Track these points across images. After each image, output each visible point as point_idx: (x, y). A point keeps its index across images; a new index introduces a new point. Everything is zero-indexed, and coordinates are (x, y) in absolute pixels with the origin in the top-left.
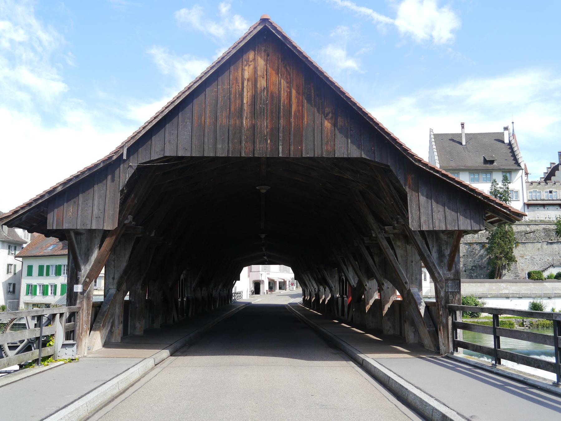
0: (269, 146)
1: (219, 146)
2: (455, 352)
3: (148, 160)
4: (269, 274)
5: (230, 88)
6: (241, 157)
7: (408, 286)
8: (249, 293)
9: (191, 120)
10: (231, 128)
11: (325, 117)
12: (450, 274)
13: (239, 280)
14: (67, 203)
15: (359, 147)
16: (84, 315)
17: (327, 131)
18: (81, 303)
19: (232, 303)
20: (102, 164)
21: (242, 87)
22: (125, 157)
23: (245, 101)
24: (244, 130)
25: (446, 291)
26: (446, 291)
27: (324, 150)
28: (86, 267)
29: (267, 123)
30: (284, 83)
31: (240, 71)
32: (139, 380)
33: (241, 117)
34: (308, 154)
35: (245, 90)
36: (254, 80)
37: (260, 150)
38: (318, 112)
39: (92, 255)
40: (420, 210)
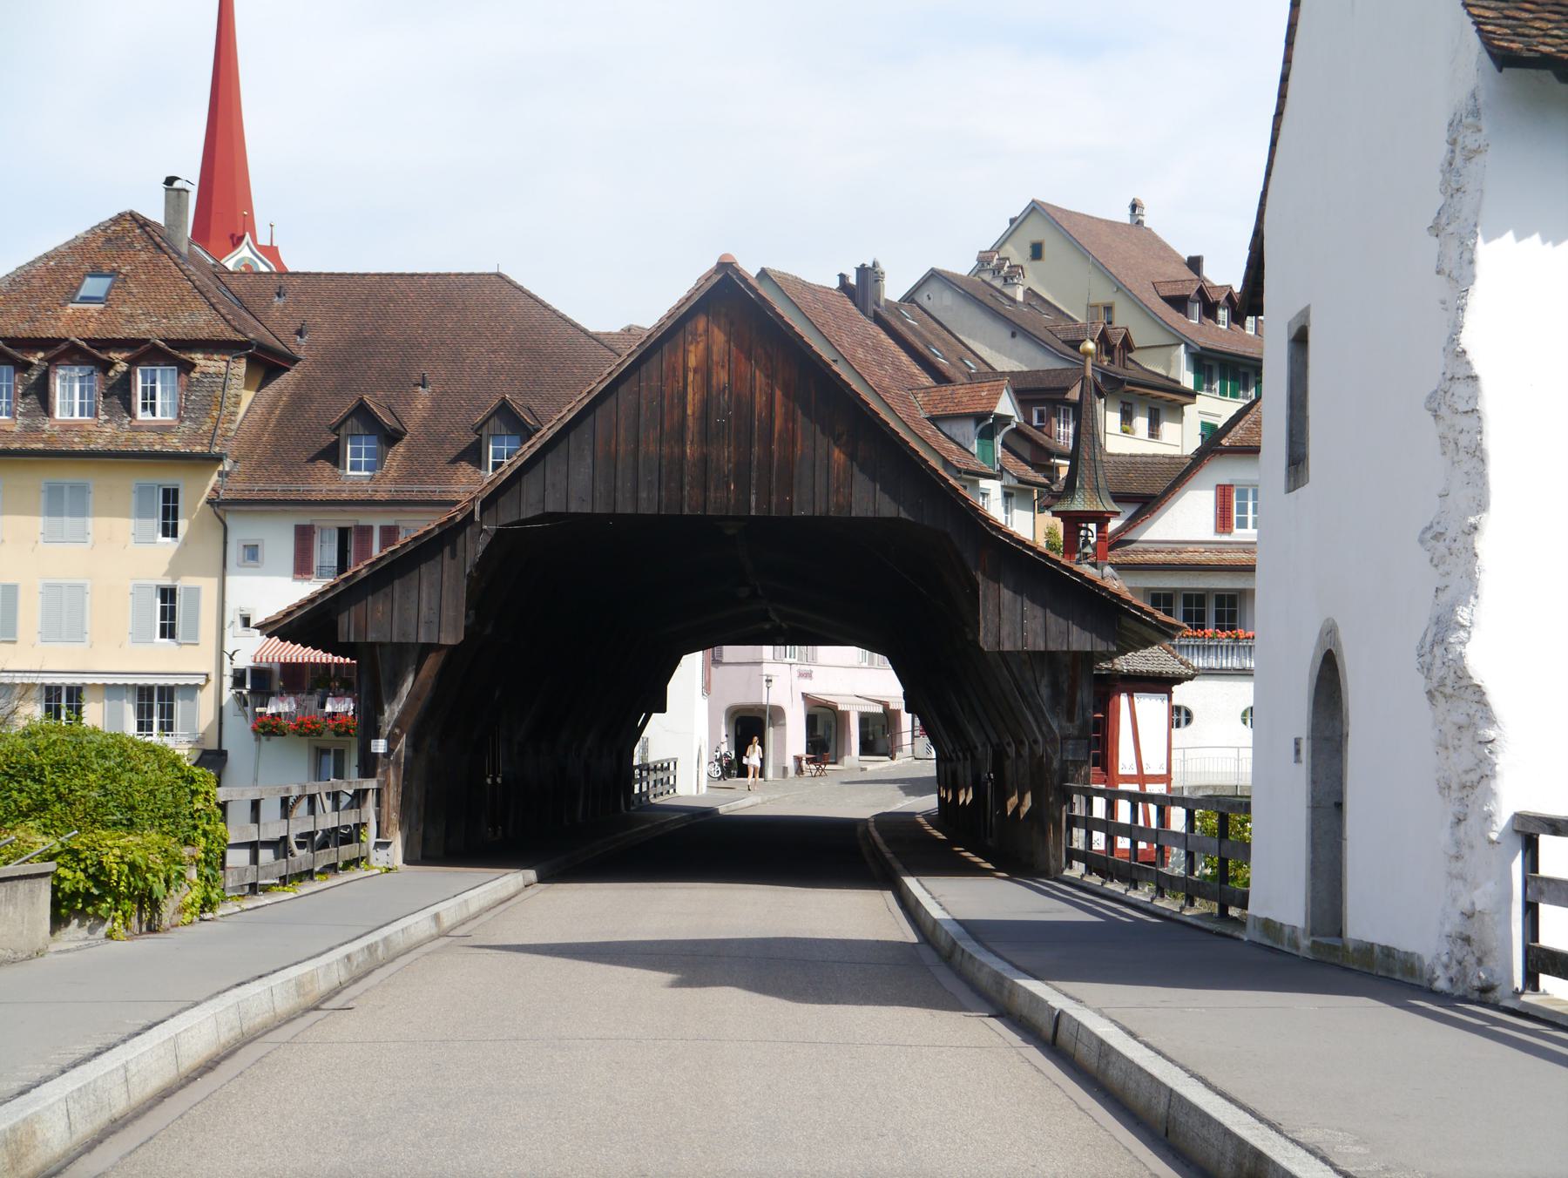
0: (732, 496)
1: (643, 495)
2: (1067, 869)
3: (515, 519)
4: (808, 675)
5: (661, 386)
6: (681, 516)
7: (1039, 747)
8: (708, 769)
9: (592, 446)
10: (664, 462)
11: (835, 443)
12: (1073, 728)
13: (663, 709)
14: (372, 595)
15: (895, 498)
16: (391, 795)
17: (838, 468)
18: (385, 773)
19: (632, 808)
20: (437, 529)
21: (684, 384)
22: (477, 518)
23: (689, 412)
24: (688, 466)
25: (1064, 758)
26: (1064, 758)
27: (831, 503)
28: (392, 707)
29: (728, 452)
30: (760, 377)
31: (680, 354)
32: (509, 899)
33: (682, 441)
34: (802, 510)
35: (690, 389)
36: (706, 370)
37: (715, 502)
38: (823, 432)
39: (403, 685)
40: (1000, 614)
